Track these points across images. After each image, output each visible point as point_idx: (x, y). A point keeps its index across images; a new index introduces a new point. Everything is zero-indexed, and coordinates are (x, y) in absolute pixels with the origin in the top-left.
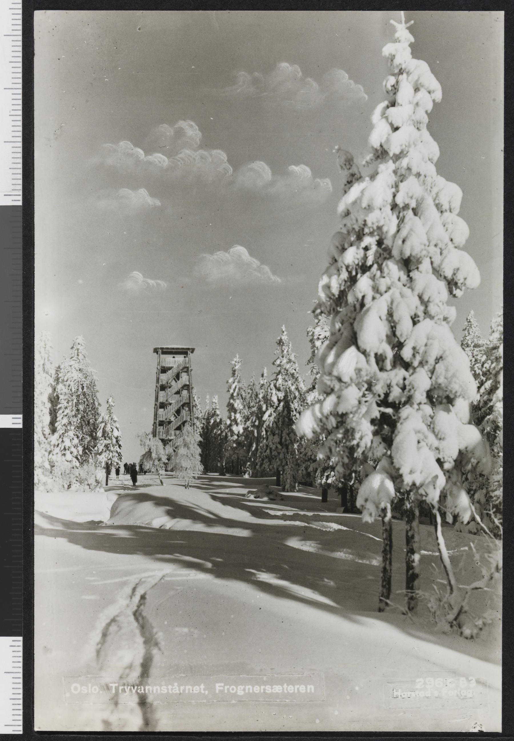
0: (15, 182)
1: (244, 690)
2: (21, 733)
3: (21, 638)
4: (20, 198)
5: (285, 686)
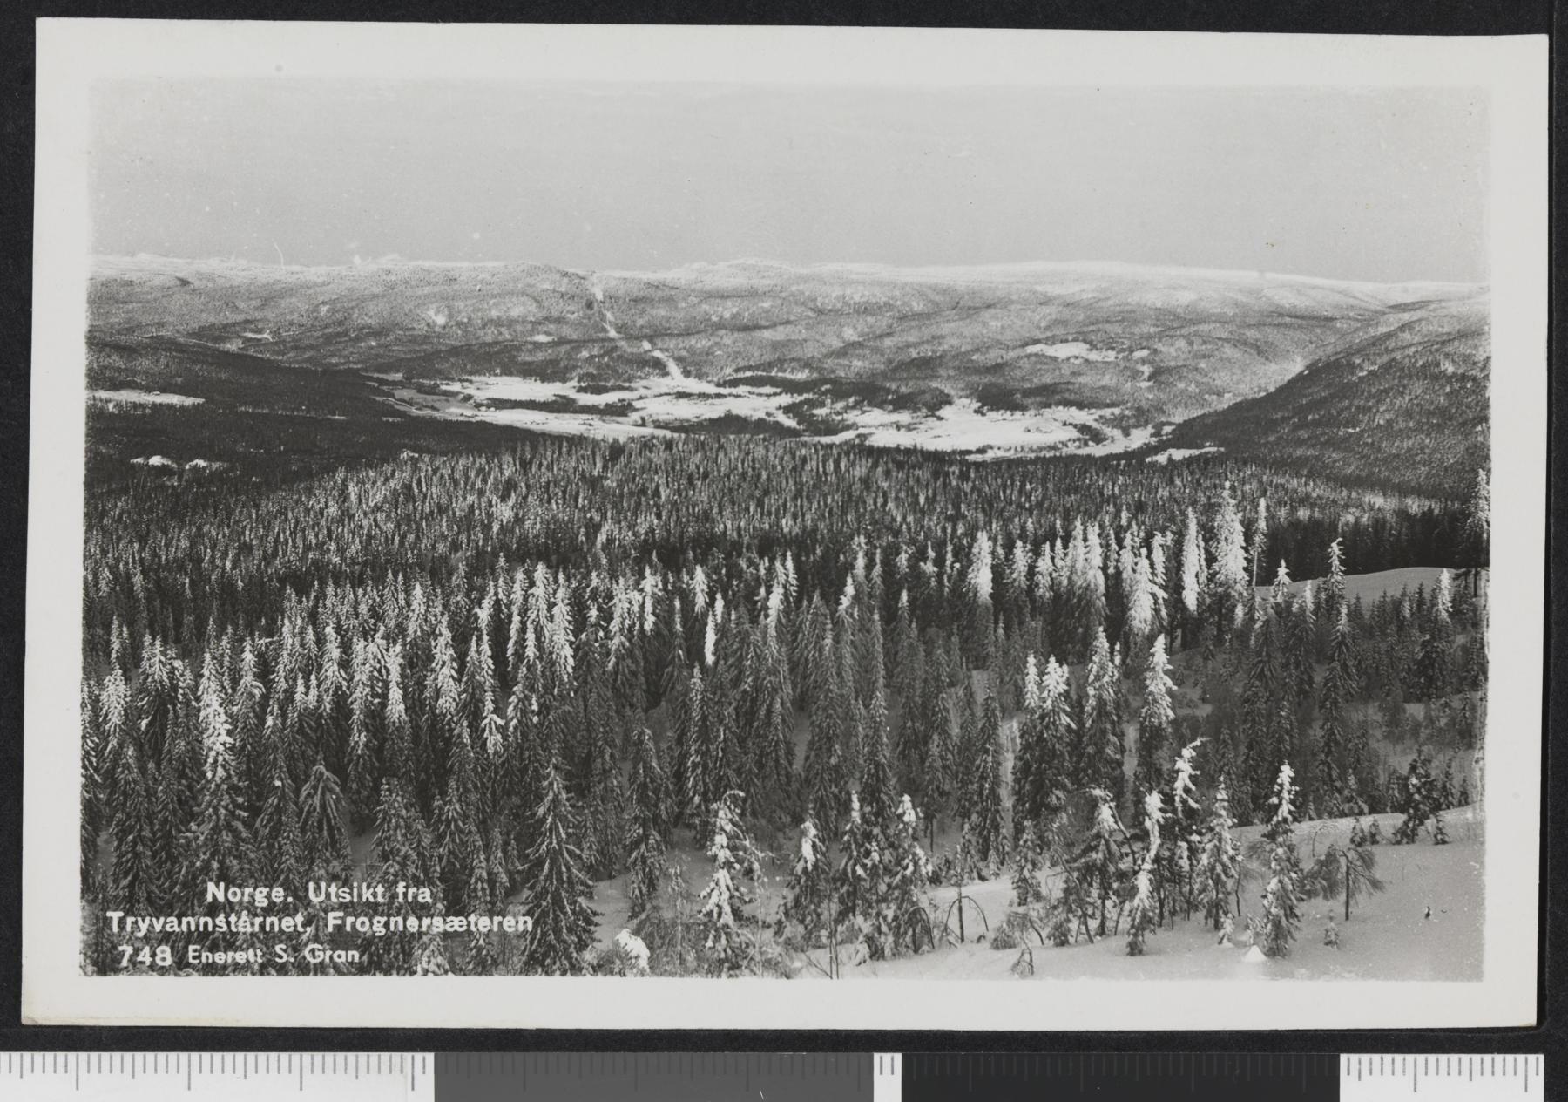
0: (385, 1068)
1: (387, 925)
2: (1541, 1057)
3: (1343, 1057)
4: (419, 1056)
5: (472, 918)
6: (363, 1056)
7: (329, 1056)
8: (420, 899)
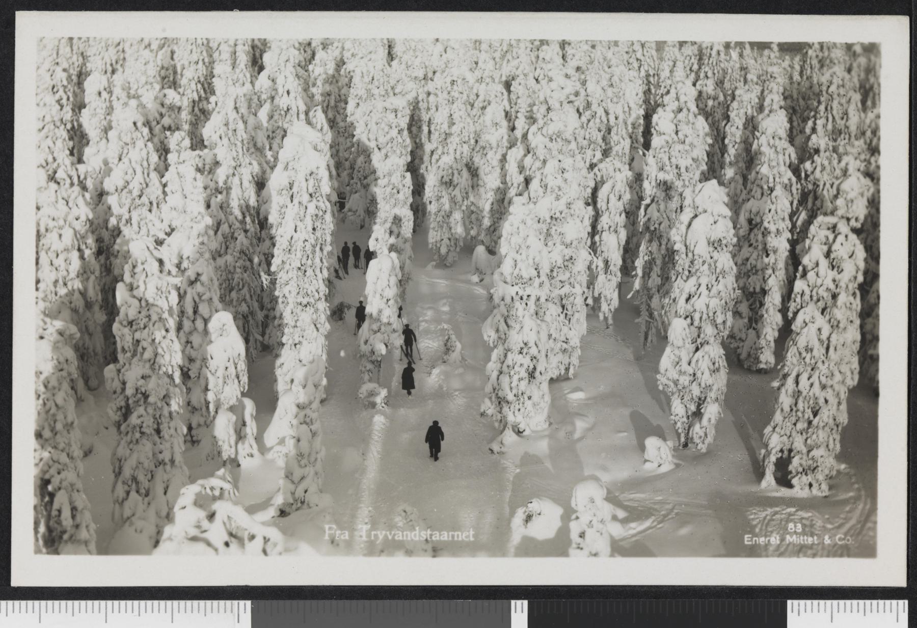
0: (222, 610)
2: (906, 602)
3: (789, 602)
4: (242, 602)
6: (209, 602)
7: (189, 602)
8: (396, 538)
